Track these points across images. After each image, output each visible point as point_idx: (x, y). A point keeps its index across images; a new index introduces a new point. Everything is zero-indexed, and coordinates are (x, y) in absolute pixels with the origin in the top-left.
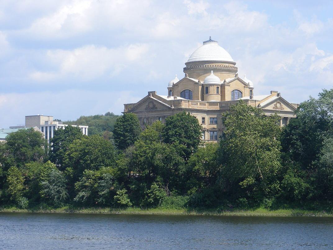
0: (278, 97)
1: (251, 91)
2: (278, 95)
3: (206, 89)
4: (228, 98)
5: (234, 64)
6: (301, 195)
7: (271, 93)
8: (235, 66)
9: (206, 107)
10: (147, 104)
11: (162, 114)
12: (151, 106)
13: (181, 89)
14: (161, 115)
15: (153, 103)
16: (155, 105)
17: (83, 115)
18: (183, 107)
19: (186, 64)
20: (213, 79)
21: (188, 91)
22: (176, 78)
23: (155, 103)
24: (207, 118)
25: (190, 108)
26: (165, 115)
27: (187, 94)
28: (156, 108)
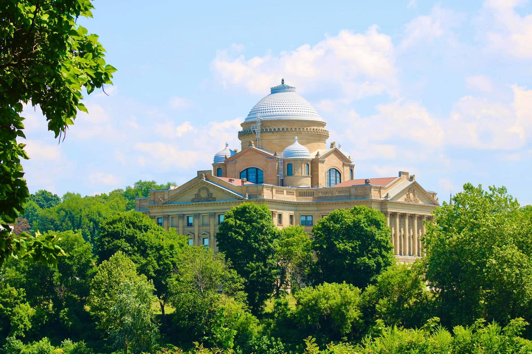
0: (411, 182)
1: (352, 171)
2: (412, 178)
3: (289, 167)
4: (323, 182)
5: (323, 124)
6: (11, 315)
7: (400, 176)
8: (325, 128)
9: (293, 199)
10: (195, 191)
11: (179, 211)
12: (204, 195)
13: (241, 166)
14: (207, 212)
15: (208, 190)
16: (212, 194)
17: (513, 193)
18: (265, 197)
19: (242, 125)
20: (301, 150)
21: (255, 170)
22: (297, 142)
23: (211, 190)
24: (286, 216)
25: (275, 198)
26: (215, 211)
27: (252, 176)
28: (214, 199)
